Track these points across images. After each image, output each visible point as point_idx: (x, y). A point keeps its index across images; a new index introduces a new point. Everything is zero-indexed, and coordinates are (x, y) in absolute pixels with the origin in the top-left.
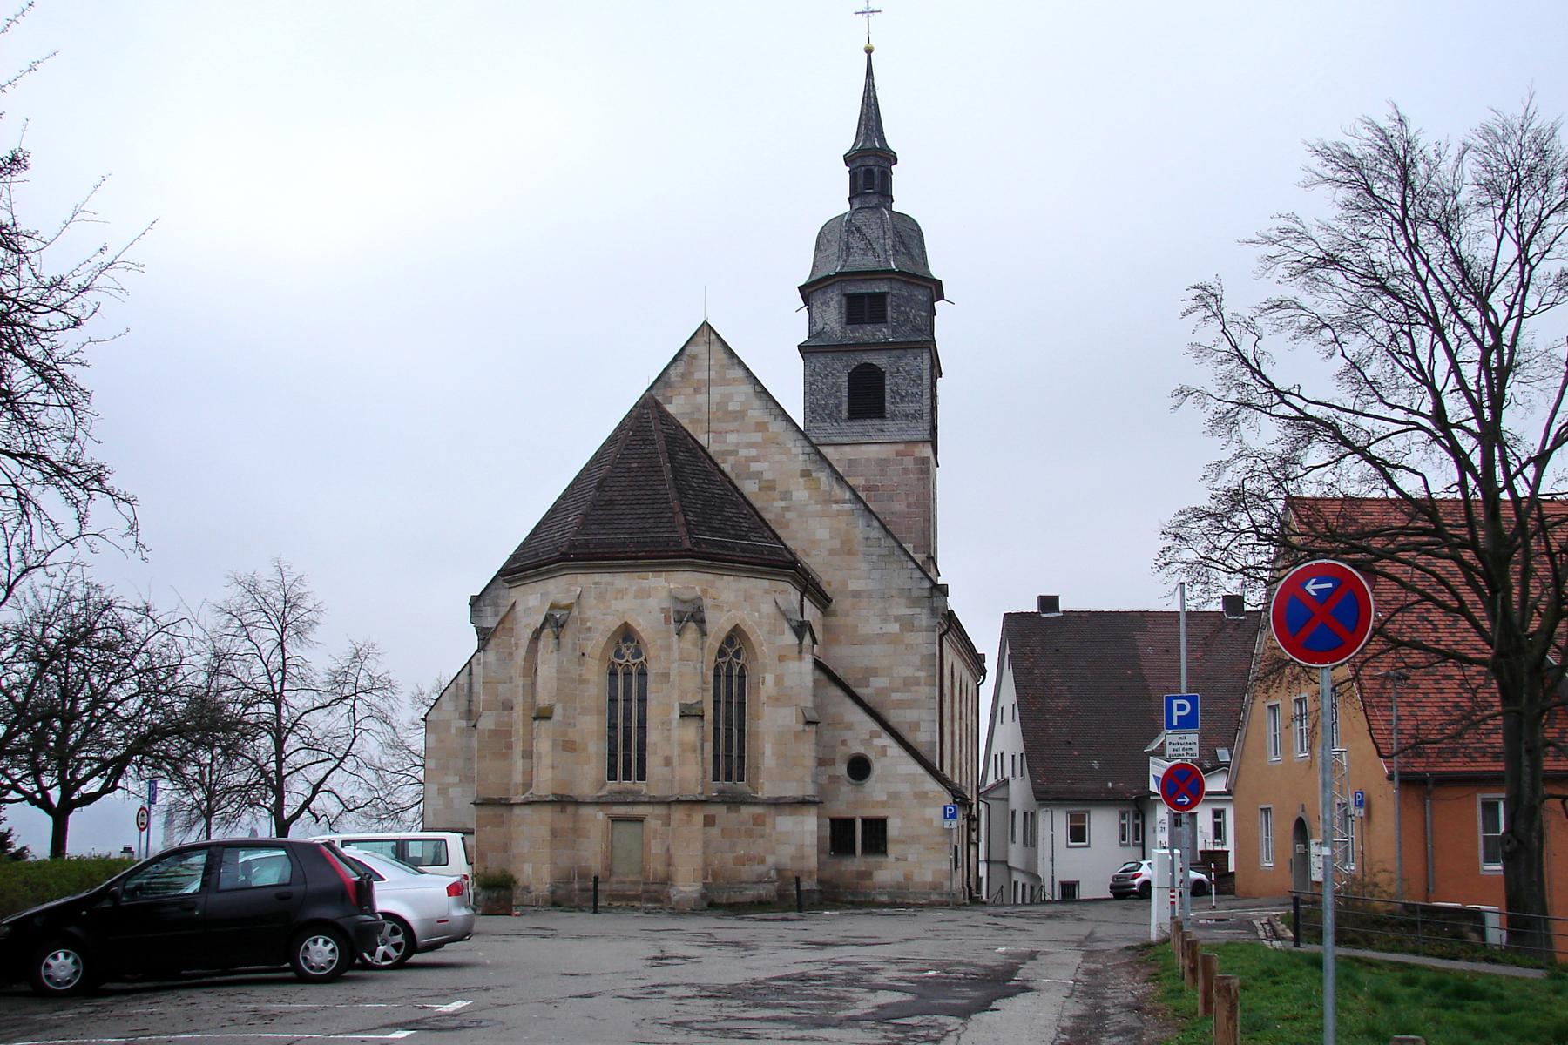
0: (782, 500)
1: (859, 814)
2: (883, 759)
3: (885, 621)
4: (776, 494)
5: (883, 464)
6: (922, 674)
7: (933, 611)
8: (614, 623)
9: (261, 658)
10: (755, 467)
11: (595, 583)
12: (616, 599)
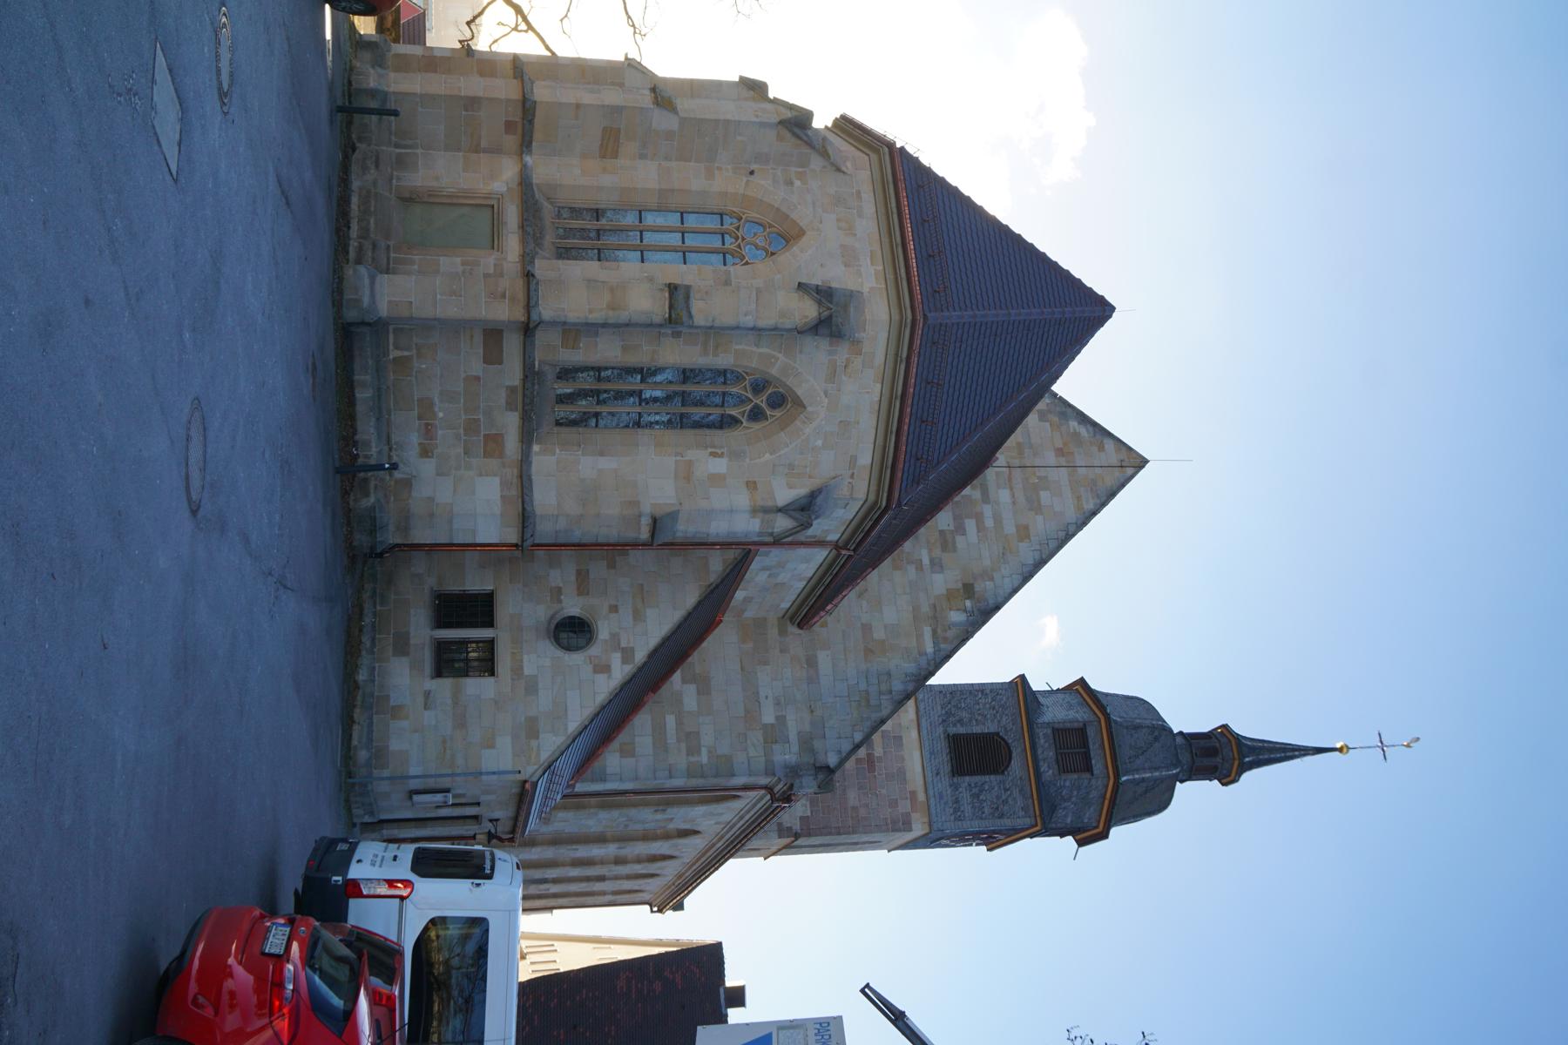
0: (932, 561)
1: (501, 634)
2: (590, 668)
3: (778, 703)
4: (937, 552)
5: (901, 775)
6: (704, 758)
7: (794, 771)
8: (802, 215)
10: (970, 525)
11: (859, 193)
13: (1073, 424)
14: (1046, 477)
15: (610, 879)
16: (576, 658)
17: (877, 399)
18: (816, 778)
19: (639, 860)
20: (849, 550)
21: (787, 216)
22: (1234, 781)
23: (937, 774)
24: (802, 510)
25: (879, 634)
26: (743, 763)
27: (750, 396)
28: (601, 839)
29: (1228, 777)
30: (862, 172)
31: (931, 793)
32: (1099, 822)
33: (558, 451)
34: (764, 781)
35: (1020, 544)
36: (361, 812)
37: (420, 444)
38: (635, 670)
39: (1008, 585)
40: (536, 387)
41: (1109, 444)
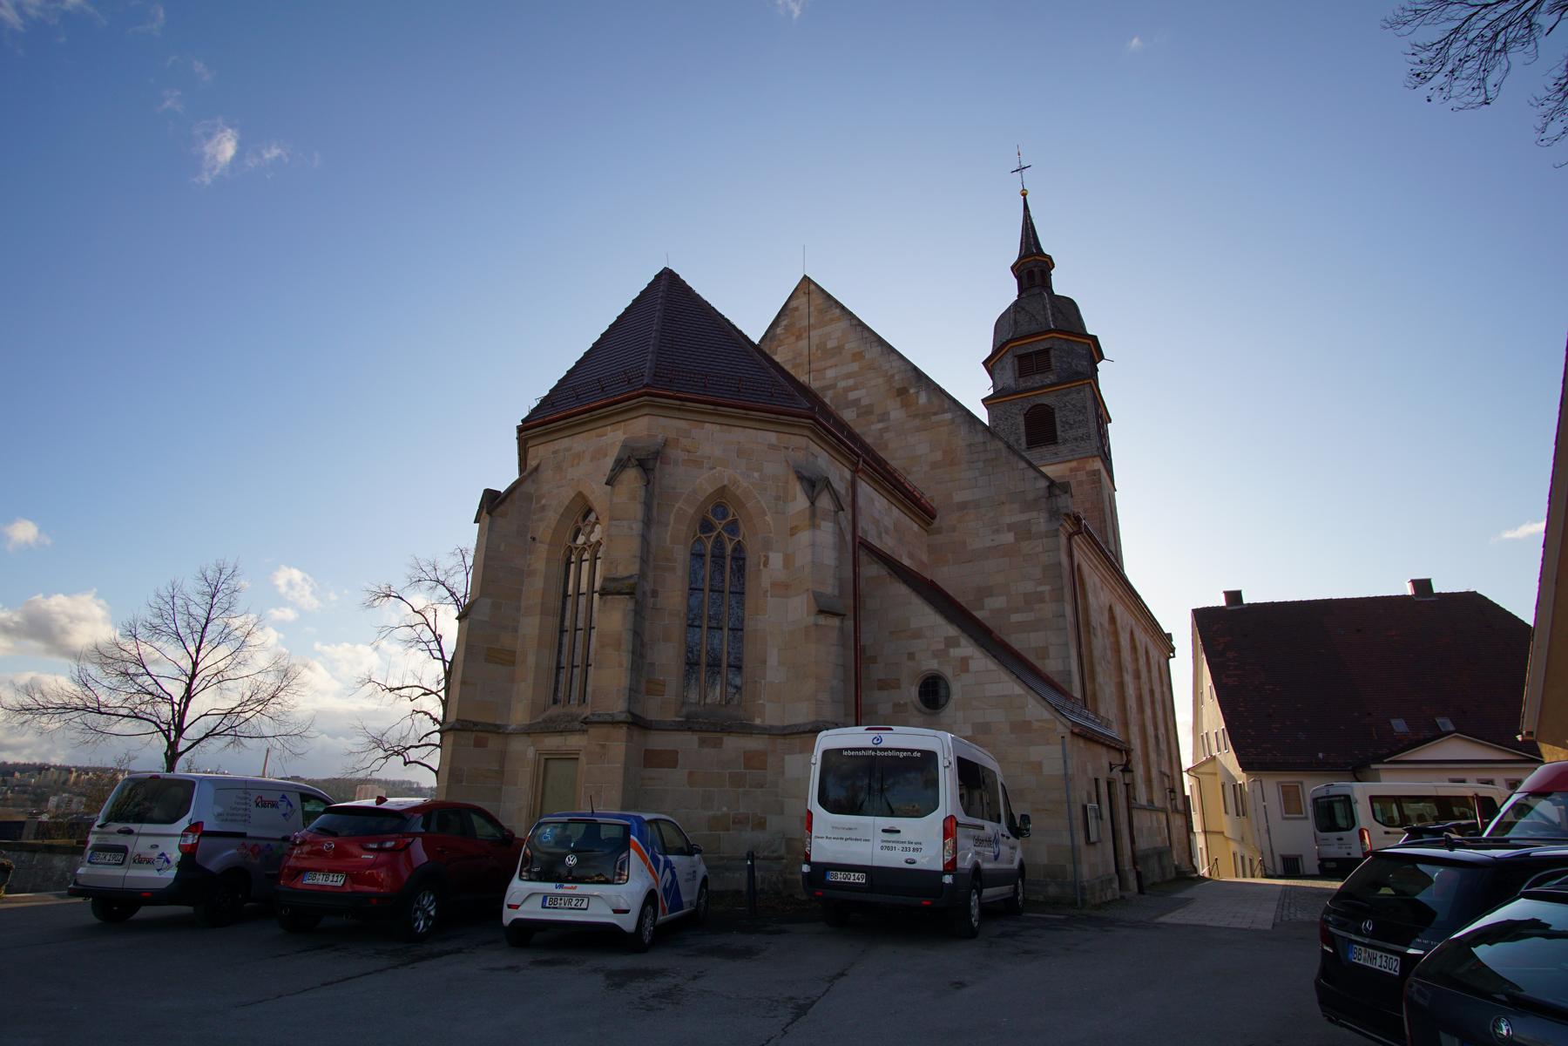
0: (879, 421)
3: (997, 531)
6: (1046, 588)
7: (1054, 514)
8: (567, 495)
9: (428, 625)
10: (852, 396)
11: (554, 453)
12: (572, 466)
13: (779, 331)
14: (817, 345)
15: (1152, 686)
16: (956, 688)
17: (718, 427)
18: (1059, 496)
19: (1136, 660)
20: (858, 461)
21: (567, 507)
22: (1050, 258)
23: (1056, 454)
24: (814, 486)
25: (938, 455)
26: (1049, 556)
27: (715, 534)
28: (1121, 686)
29: (1047, 264)
30: (539, 452)
31: (1070, 458)
32: (1085, 343)
33: (761, 702)
34: (1063, 540)
35: (866, 357)
36: (1109, 893)
37: (752, 829)
38: (966, 635)
39: (897, 363)
40: (701, 720)
41: (794, 304)
